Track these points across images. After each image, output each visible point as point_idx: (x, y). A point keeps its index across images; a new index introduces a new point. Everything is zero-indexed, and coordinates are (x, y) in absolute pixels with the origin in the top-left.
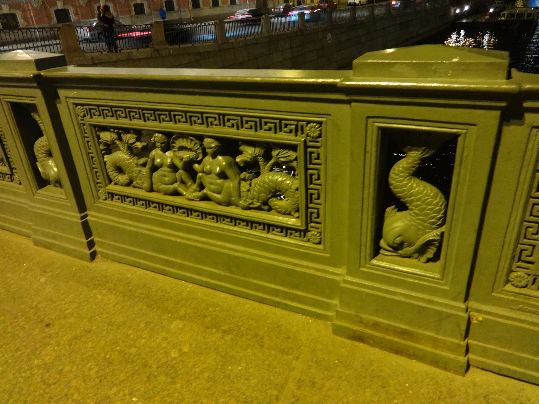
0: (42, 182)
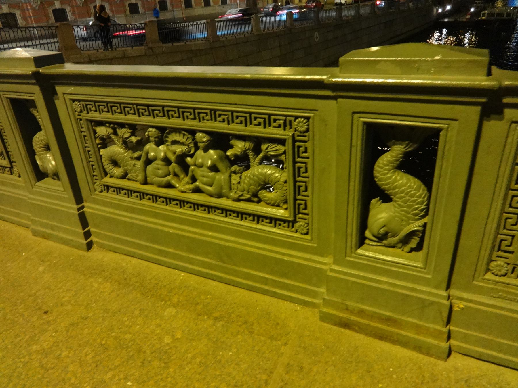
0: (40, 174)
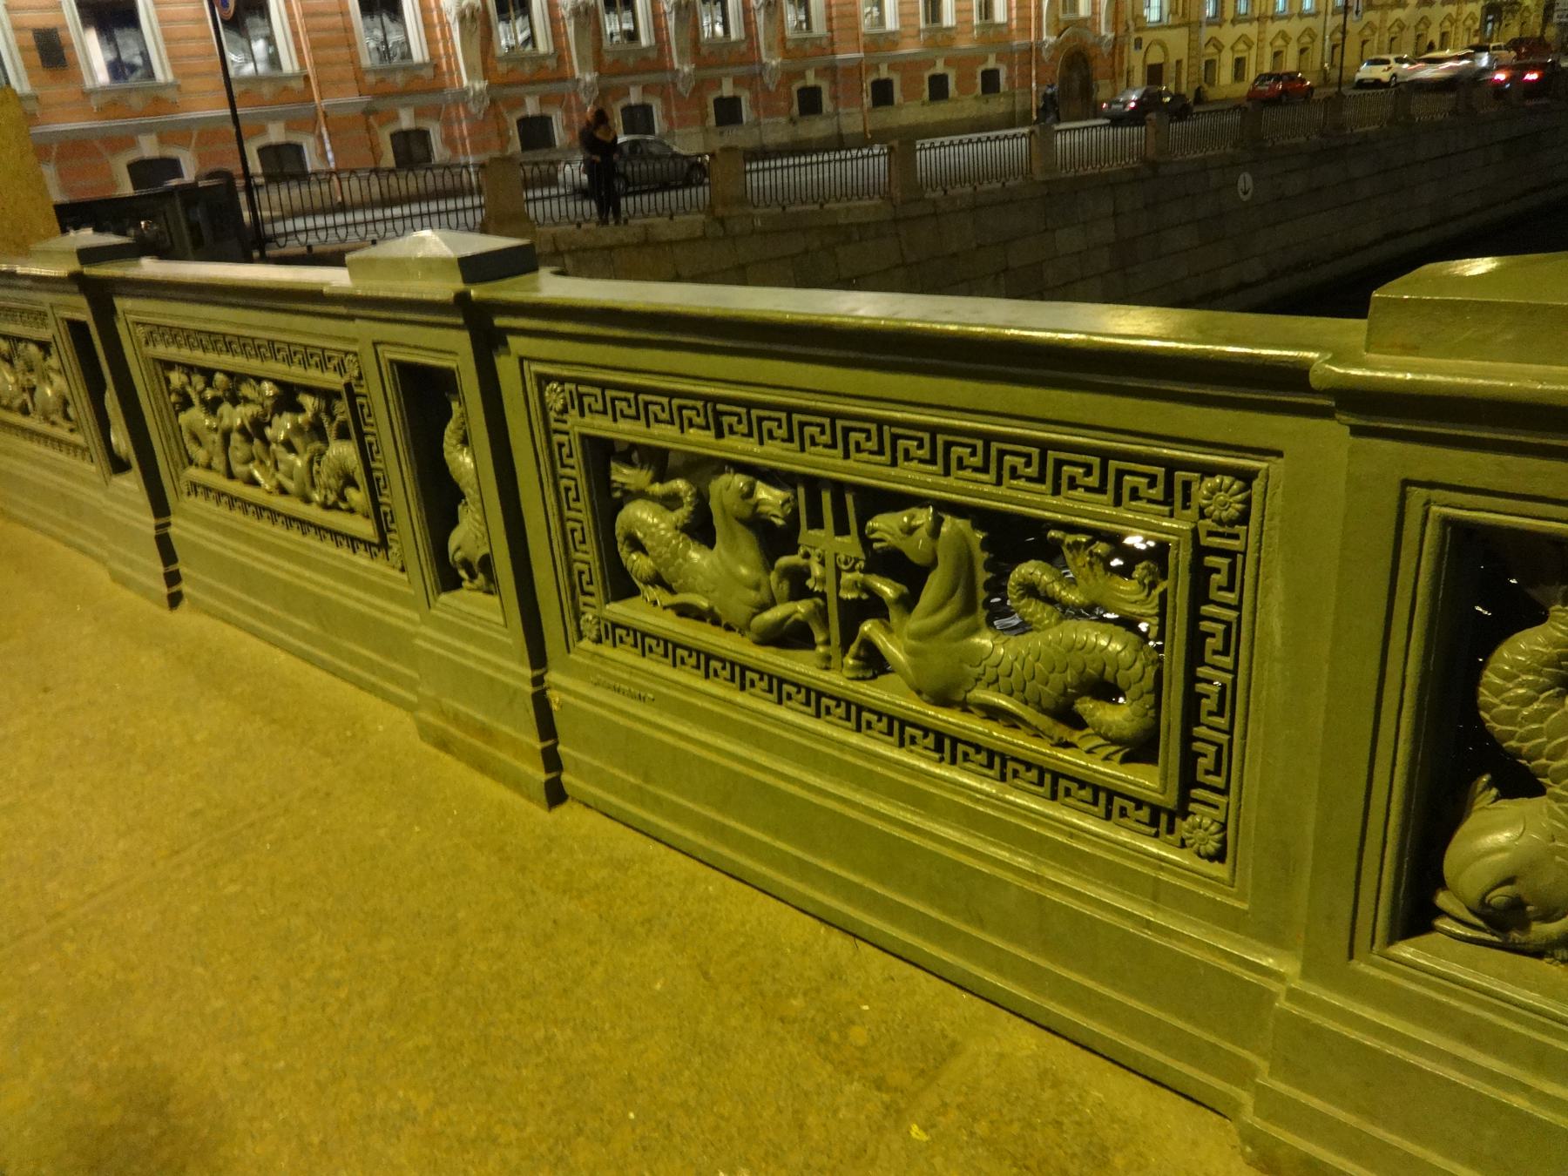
0: (448, 579)
